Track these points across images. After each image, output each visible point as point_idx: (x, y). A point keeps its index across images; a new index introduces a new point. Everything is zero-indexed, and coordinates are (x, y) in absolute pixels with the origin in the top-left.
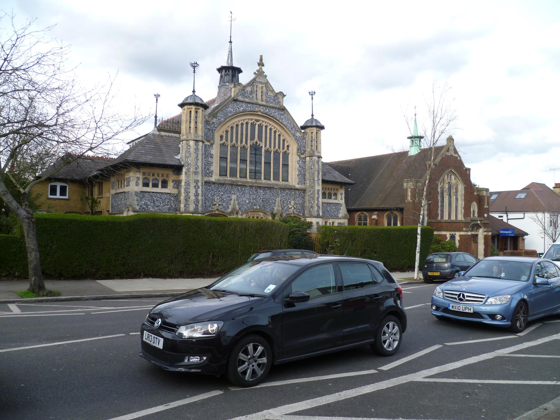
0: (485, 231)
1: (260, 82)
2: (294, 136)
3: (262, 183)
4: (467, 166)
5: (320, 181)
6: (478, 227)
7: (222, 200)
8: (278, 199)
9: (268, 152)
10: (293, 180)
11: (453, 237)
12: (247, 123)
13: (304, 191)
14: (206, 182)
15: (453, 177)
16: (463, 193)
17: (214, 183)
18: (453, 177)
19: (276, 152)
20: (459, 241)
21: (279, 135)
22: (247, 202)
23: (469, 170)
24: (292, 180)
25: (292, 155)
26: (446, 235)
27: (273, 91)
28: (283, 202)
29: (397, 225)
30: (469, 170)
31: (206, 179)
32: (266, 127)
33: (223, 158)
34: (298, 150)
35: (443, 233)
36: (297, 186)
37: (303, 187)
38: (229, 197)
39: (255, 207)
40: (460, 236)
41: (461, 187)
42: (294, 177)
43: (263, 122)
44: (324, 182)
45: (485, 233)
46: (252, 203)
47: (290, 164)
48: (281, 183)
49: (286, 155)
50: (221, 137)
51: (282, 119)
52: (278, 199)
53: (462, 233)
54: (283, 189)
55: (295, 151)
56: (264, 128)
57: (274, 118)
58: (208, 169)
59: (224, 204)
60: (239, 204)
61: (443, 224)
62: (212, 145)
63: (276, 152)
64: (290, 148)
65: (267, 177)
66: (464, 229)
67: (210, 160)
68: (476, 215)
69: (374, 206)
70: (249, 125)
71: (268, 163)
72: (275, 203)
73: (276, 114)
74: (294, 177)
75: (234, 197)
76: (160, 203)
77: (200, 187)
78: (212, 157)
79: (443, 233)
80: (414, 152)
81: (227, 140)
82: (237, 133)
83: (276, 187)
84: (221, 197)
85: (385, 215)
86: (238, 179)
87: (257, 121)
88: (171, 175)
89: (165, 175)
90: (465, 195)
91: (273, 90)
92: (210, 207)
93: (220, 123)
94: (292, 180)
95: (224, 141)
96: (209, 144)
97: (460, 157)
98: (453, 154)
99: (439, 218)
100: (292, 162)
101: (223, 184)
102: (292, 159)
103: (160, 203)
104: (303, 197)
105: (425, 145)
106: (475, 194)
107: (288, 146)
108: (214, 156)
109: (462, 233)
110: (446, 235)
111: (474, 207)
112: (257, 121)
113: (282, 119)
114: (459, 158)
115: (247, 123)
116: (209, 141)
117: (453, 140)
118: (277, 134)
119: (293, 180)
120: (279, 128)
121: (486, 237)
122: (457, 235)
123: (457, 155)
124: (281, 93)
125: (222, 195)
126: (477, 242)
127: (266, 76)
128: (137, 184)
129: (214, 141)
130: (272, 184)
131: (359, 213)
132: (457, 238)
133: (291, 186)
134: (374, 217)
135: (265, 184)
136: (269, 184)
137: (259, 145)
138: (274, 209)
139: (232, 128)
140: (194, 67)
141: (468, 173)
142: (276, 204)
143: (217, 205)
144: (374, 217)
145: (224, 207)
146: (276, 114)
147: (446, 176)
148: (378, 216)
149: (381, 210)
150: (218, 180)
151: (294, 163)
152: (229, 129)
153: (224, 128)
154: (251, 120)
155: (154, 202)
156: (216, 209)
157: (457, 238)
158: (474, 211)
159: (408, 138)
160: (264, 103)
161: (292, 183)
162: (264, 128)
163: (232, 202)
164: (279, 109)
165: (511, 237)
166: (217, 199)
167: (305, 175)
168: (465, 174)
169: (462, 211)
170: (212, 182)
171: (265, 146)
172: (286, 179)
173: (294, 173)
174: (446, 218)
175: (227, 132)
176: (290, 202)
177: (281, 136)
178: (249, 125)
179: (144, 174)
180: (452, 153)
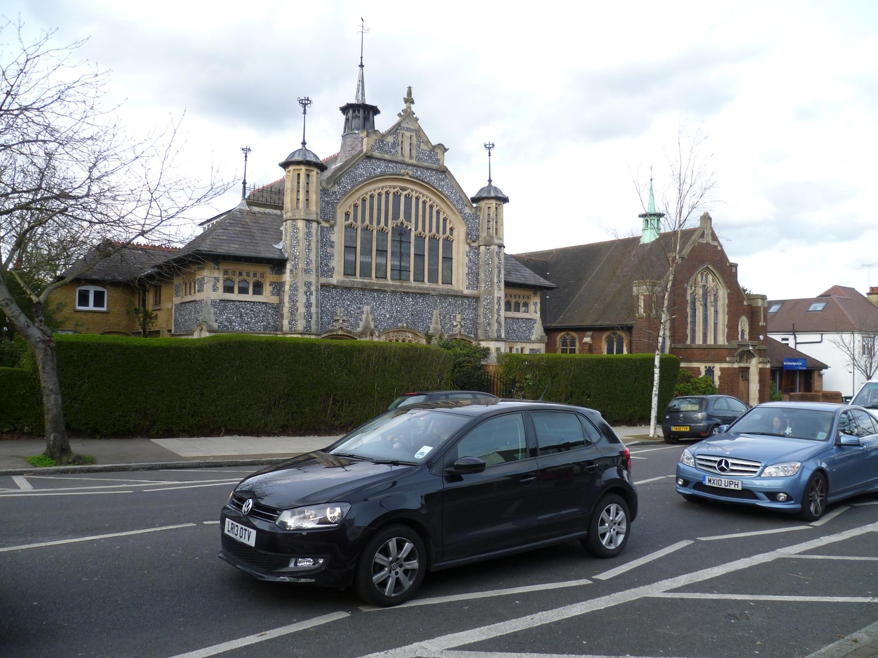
0: (760, 363)
1: (408, 129)
2: (461, 213)
3: (411, 287)
4: (732, 259)
5: (502, 284)
6: (749, 355)
7: (349, 314)
8: (436, 313)
9: (420, 238)
10: (460, 282)
11: (710, 371)
12: (387, 193)
13: (477, 299)
14: (322, 286)
15: (710, 277)
16: (726, 302)
17: (335, 287)
18: (710, 277)
19: (433, 239)
20: (720, 378)
22: (388, 316)
23: (736, 266)
24: (458, 281)
25: (458, 243)
26: (699, 368)
27: (428, 142)
28: (444, 317)
29: (622, 352)
30: (736, 266)
31: (323, 280)
32: (417, 199)
33: (350, 248)
34: (468, 234)
35: (695, 365)
36: (466, 292)
37: (475, 292)
38: (359, 308)
39: (400, 325)
40: (722, 369)
41: (723, 293)
42: (461, 277)
43: (412, 190)
44: (508, 284)
45: (761, 366)
46: (395, 318)
47: (454, 256)
48: (440, 286)
49: (448, 243)
50: (347, 214)
51: (443, 186)
52: (436, 313)
53: (725, 365)
54: (444, 296)
55: (463, 236)
56: (414, 200)
57: (429, 184)
58: (327, 265)
59: (352, 320)
60: (374, 320)
61: (695, 351)
62: (332, 226)
63: (433, 239)
64: (455, 232)
65: (419, 278)
66: (728, 359)
67: (329, 250)
68: (747, 337)
69: (587, 323)
70: (391, 196)
71: (419, 256)
72: (430, 319)
73: (433, 178)
74: (461, 277)
75: (366, 308)
76: (251, 318)
77: (314, 293)
78: (332, 246)
79: (695, 365)
80: (648, 237)
81: (355, 220)
82: (372, 208)
83: (433, 293)
84: (346, 309)
85: (604, 336)
87: (403, 189)
88: (268, 275)
89: (259, 275)
90: (729, 306)
91: (428, 141)
92: (329, 324)
93: (346, 192)
94: (458, 281)
95: (351, 220)
96: (327, 225)
97: (721, 246)
98: (710, 241)
99: (689, 342)
100: (458, 254)
101: (349, 289)
102: (458, 249)
103: (251, 318)
104: (476, 309)
105: (666, 227)
106: (745, 303)
107: (451, 229)
108: (336, 245)
109: (725, 365)
110: (699, 368)
111: (744, 324)
112: (403, 189)
113: (443, 186)
114: (719, 248)
115: (387, 193)
116: (328, 221)
117: (710, 219)
118: (435, 210)
119: (460, 282)
120: (437, 201)
121: (761, 372)
122: (717, 367)
123: (716, 244)
124: (440, 146)
125: (348, 305)
126: (748, 380)
127: (417, 119)
128: (215, 289)
129: (335, 221)
130: (427, 289)
131: (563, 333)
132: (717, 373)
133: (457, 292)
134: (587, 340)
135: (415, 288)
137: (407, 227)
138: (429, 327)
139: (364, 200)
140: (305, 105)
141: (734, 270)
142: (433, 320)
143: (341, 321)
144: (587, 340)
145: (351, 325)
146: (433, 178)
147: (699, 276)
148: (593, 338)
149: (598, 330)
150: (342, 282)
151: (461, 255)
152: (360, 203)
153: (351, 201)
154: (394, 188)
155: (241, 316)
156: (338, 327)
157: (717, 373)
158: (743, 331)
159: (640, 216)
160: (414, 162)
161: (458, 286)
162: (414, 200)
163: (364, 316)
164: (437, 170)
165: (801, 371)
166: (341, 312)
167: (478, 274)
168: (729, 273)
169: (724, 331)
170: (332, 285)
171: (416, 229)
172: (448, 281)
173: (460, 271)
174: (699, 341)
175: (356, 206)
176: (455, 317)
177: (441, 213)
178: (391, 196)
179: (226, 272)
180: (708, 239)
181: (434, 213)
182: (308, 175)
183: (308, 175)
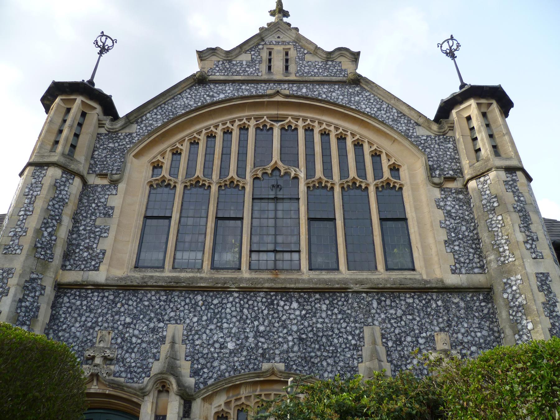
3: (303, 281)
5: (69, 145)
7: (125, 343)
8: (371, 333)
9: (321, 190)
10: (433, 259)
13: (487, 292)
17: (98, 287)
19: (355, 190)
21: (376, 155)
24: (427, 261)
25: (415, 189)
27: (317, 50)
28: (399, 341)
31: (72, 276)
32: (309, 130)
33: (153, 218)
34: (431, 170)
36: (452, 280)
37: (479, 279)
39: (266, 366)
42: (433, 251)
43: (297, 119)
44: (405, 219)
46: (250, 350)
47: (410, 214)
48: (381, 275)
49: (391, 191)
50: (157, 166)
51: (359, 103)
52: (371, 333)
54: (395, 291)
55: (421, 173)
56: (301, 133)
57: (328, 102)
59: (131, 358)
60: (192, 357)
63: (355, 190)
64: (404, 173)
70: (252, 132)
71: (321, 220)
72: (356, 347)
73: (337, 95)
74: (433, 251)
75: (174, 330)
78: (108, 215)
82: (226, 154)
83: (357, 288)
86: (344, 273)
87: (276, 119)
91: (317, 48)
94: (427, 261)
96: (105, 182)
100: (417, 209)
102: (416, 200)
104: (491, 317)
107: (395, 169)
112: (276, 119)
118: (349, 141)
119: (433, 259)
120: (355, 128)
124: (342, 51)
125: (127, 325)
127: (297, 29)
130: (345, 281)
133: (426, 282)
135: (310, 281)
136: (160, 279)
138: (354, 370)
142: (366, 351)
143: (98, 361)
145: (129, 369)
146: (337, 95)
151: (426, 210)
160: (292, 77)
162: (301, 133)
163: (165, 349)
164: (342, 83)
167: (477, 240)
173: (431, 240)
176: (431, 340)
177: (366, 147)
178: (252, 132)
181: (317, 138)
182: (84, 115)
183: (84, 115)
